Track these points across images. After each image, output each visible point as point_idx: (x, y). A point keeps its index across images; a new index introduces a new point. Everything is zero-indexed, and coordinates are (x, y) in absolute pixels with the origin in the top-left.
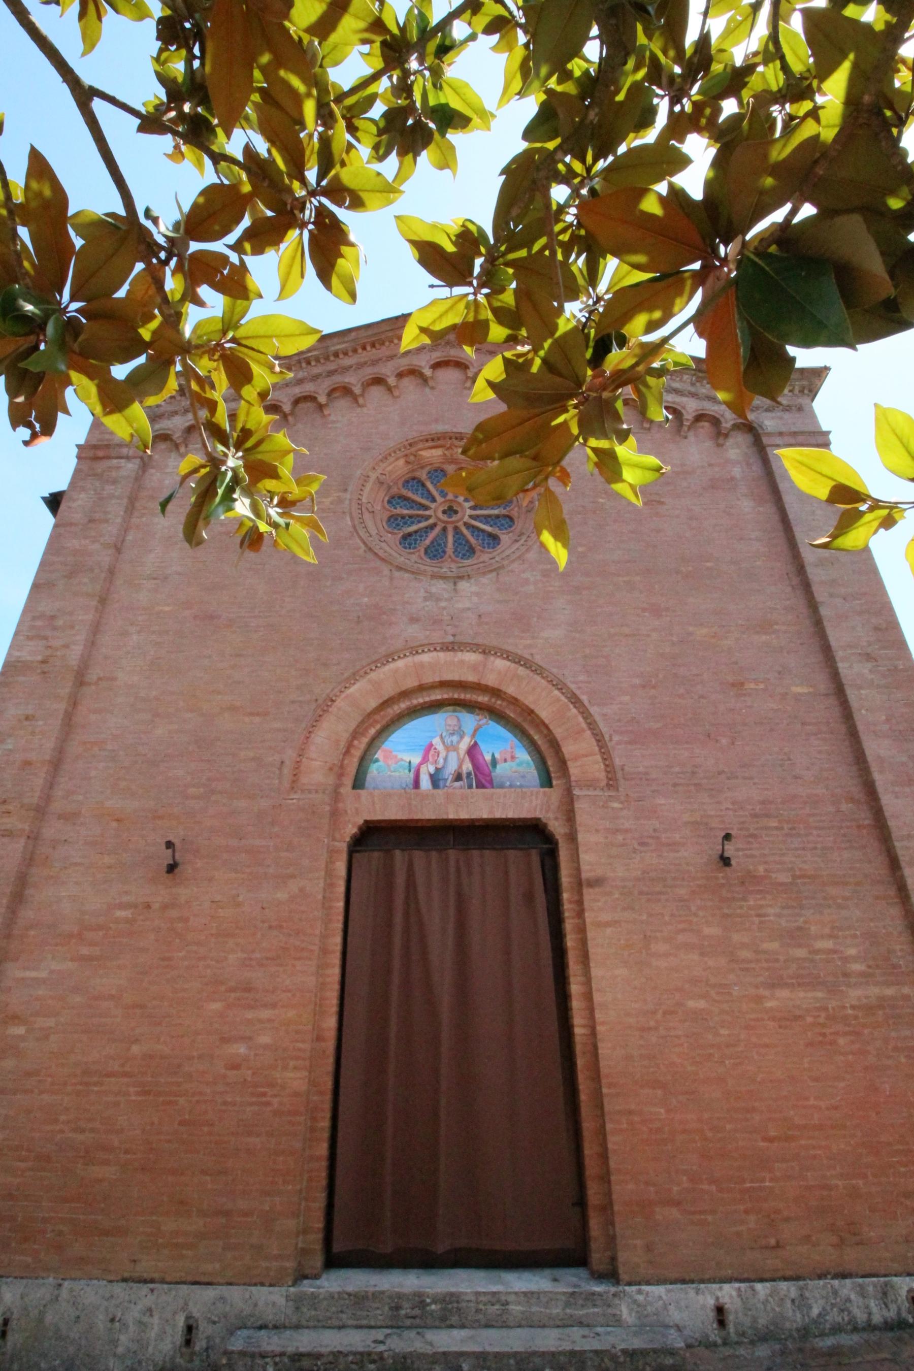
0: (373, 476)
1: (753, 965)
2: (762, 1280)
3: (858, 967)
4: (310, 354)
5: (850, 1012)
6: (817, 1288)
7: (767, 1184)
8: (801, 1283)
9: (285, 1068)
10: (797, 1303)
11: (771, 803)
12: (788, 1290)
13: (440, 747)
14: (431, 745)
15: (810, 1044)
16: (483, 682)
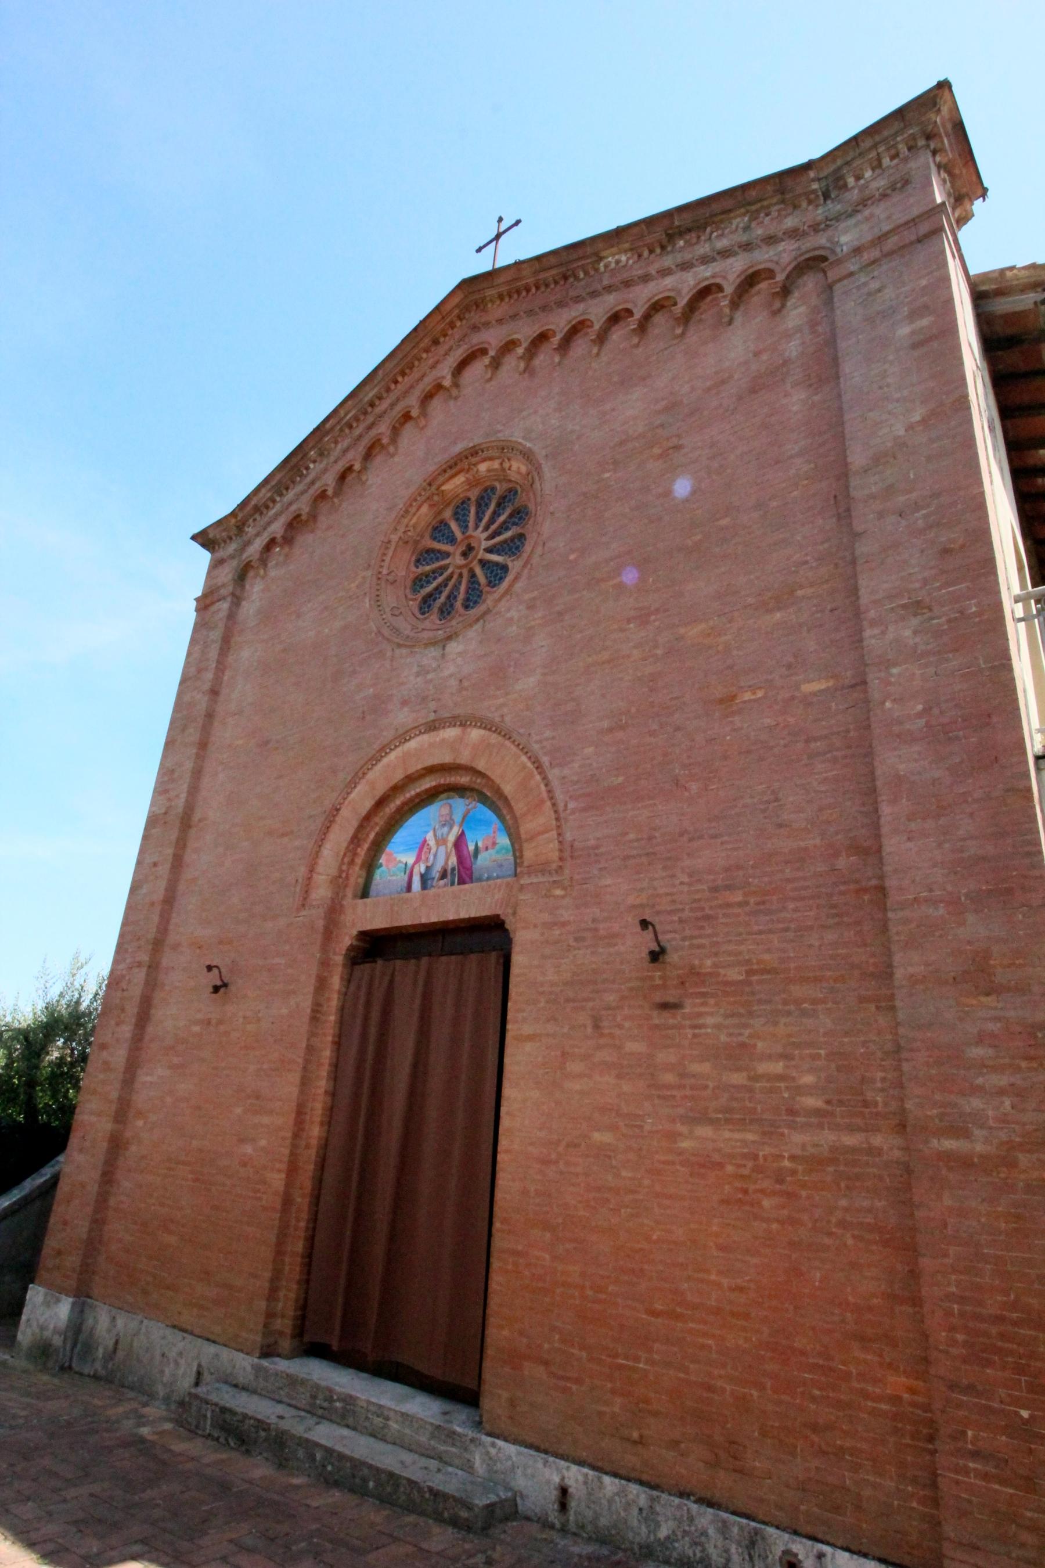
0: (394, 538)
1: (674, 1093)
2: (615, 1475)
3: (811, 1102)
4: (348, 418)
5: (786, 1163)
6: (671, 1506)
7: (641, 1365)
8: (655, 1493)
10: (644, 1515)
11: (739, 867)
12: (638, 1496)
13: (432, 842)
14: (425, 841)
15: (724, 1202)
16: (458, 761)
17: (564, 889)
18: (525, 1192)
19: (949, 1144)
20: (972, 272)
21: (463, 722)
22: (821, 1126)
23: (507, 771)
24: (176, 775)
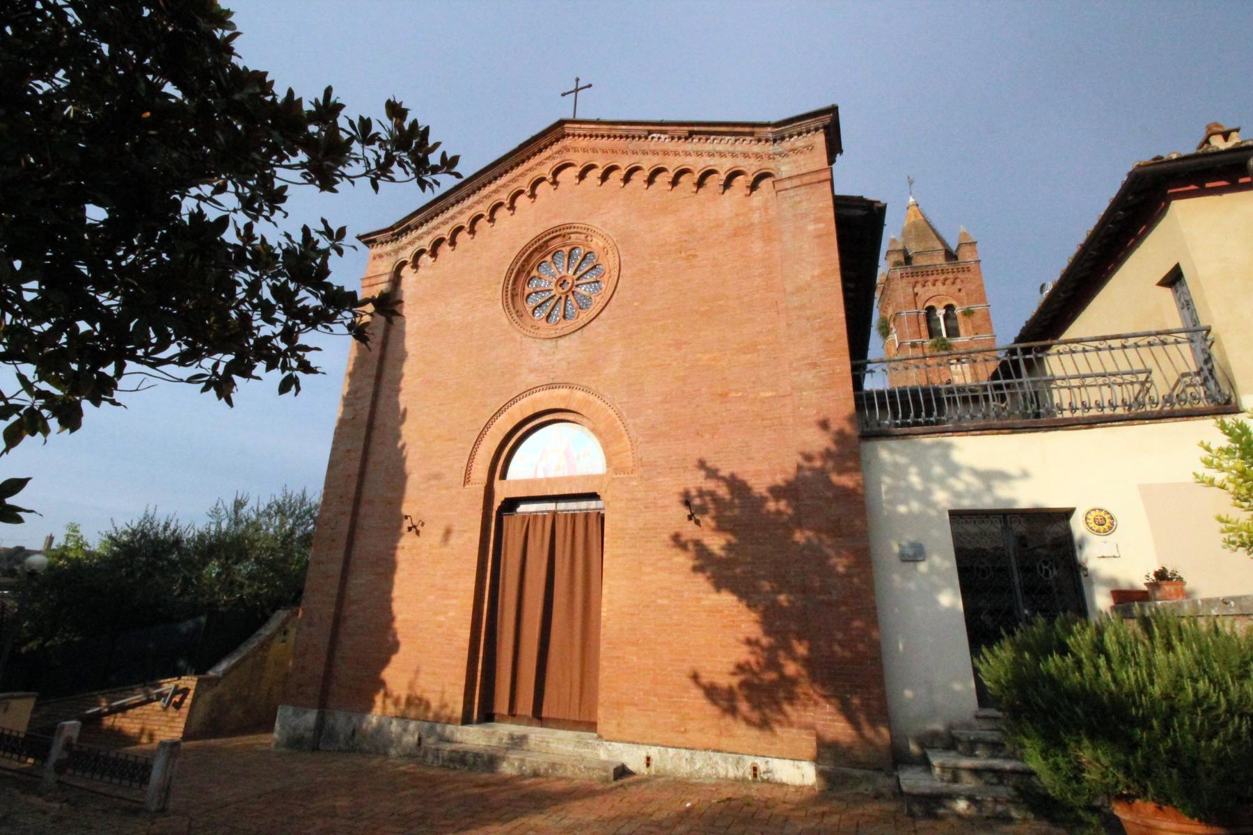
18: (622, 629)
19: (822, 597)
20: (837, 193)
21: (570, 386)
23: (576, 398)
24: (359, 394)
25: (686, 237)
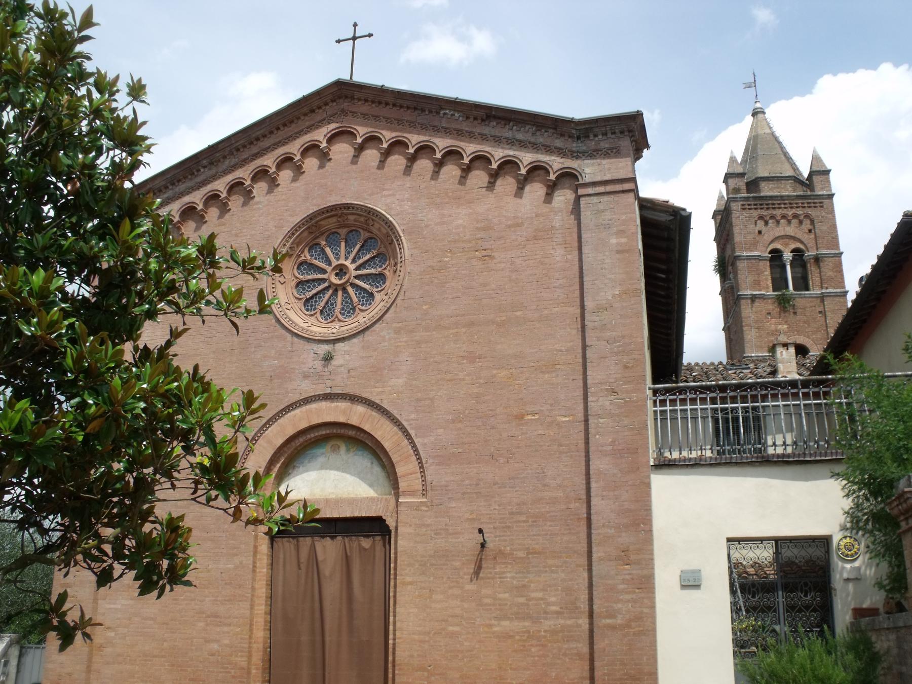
3: (554, 608)
9: (236, 656)
11: (524, 504)
15: (516, 651)
17: (427, 507)
18: (412, 656)
19: (608, 621)
22: (558, 618)
25: (481, 234)
